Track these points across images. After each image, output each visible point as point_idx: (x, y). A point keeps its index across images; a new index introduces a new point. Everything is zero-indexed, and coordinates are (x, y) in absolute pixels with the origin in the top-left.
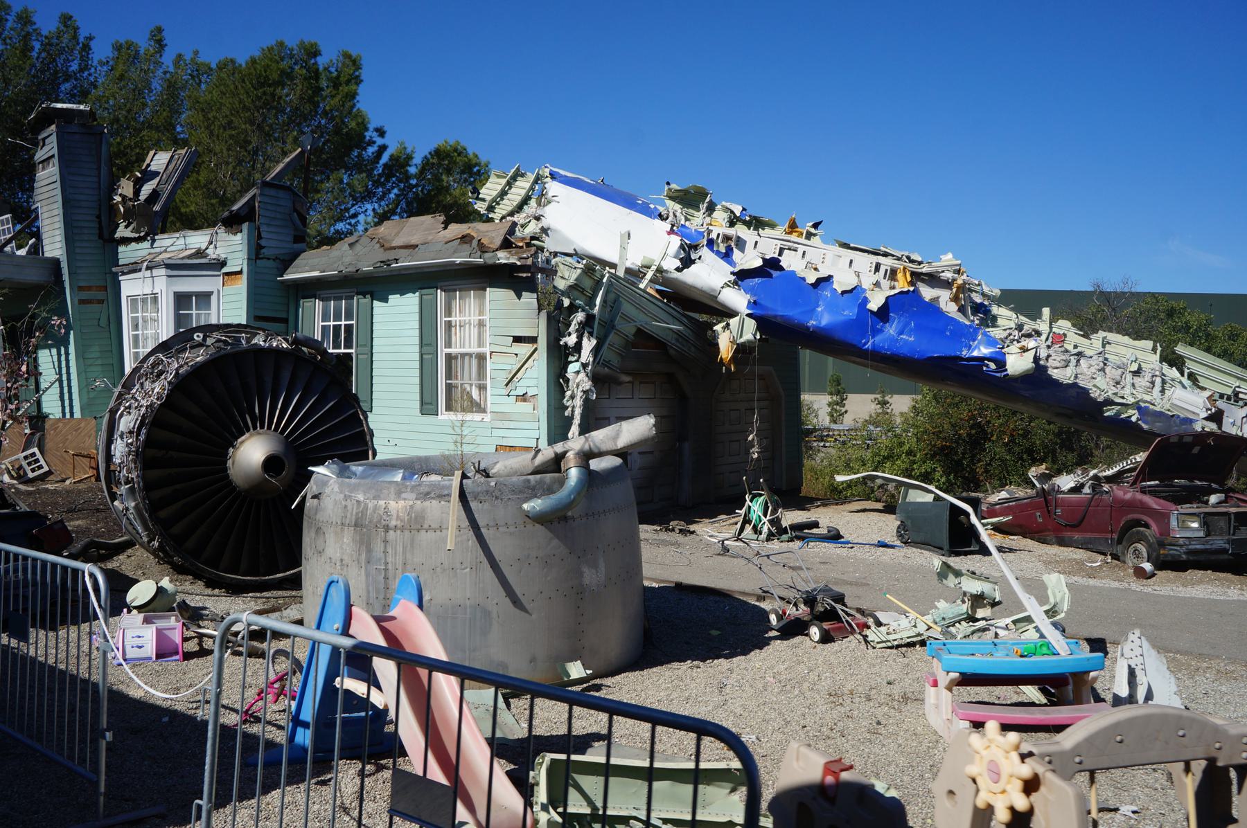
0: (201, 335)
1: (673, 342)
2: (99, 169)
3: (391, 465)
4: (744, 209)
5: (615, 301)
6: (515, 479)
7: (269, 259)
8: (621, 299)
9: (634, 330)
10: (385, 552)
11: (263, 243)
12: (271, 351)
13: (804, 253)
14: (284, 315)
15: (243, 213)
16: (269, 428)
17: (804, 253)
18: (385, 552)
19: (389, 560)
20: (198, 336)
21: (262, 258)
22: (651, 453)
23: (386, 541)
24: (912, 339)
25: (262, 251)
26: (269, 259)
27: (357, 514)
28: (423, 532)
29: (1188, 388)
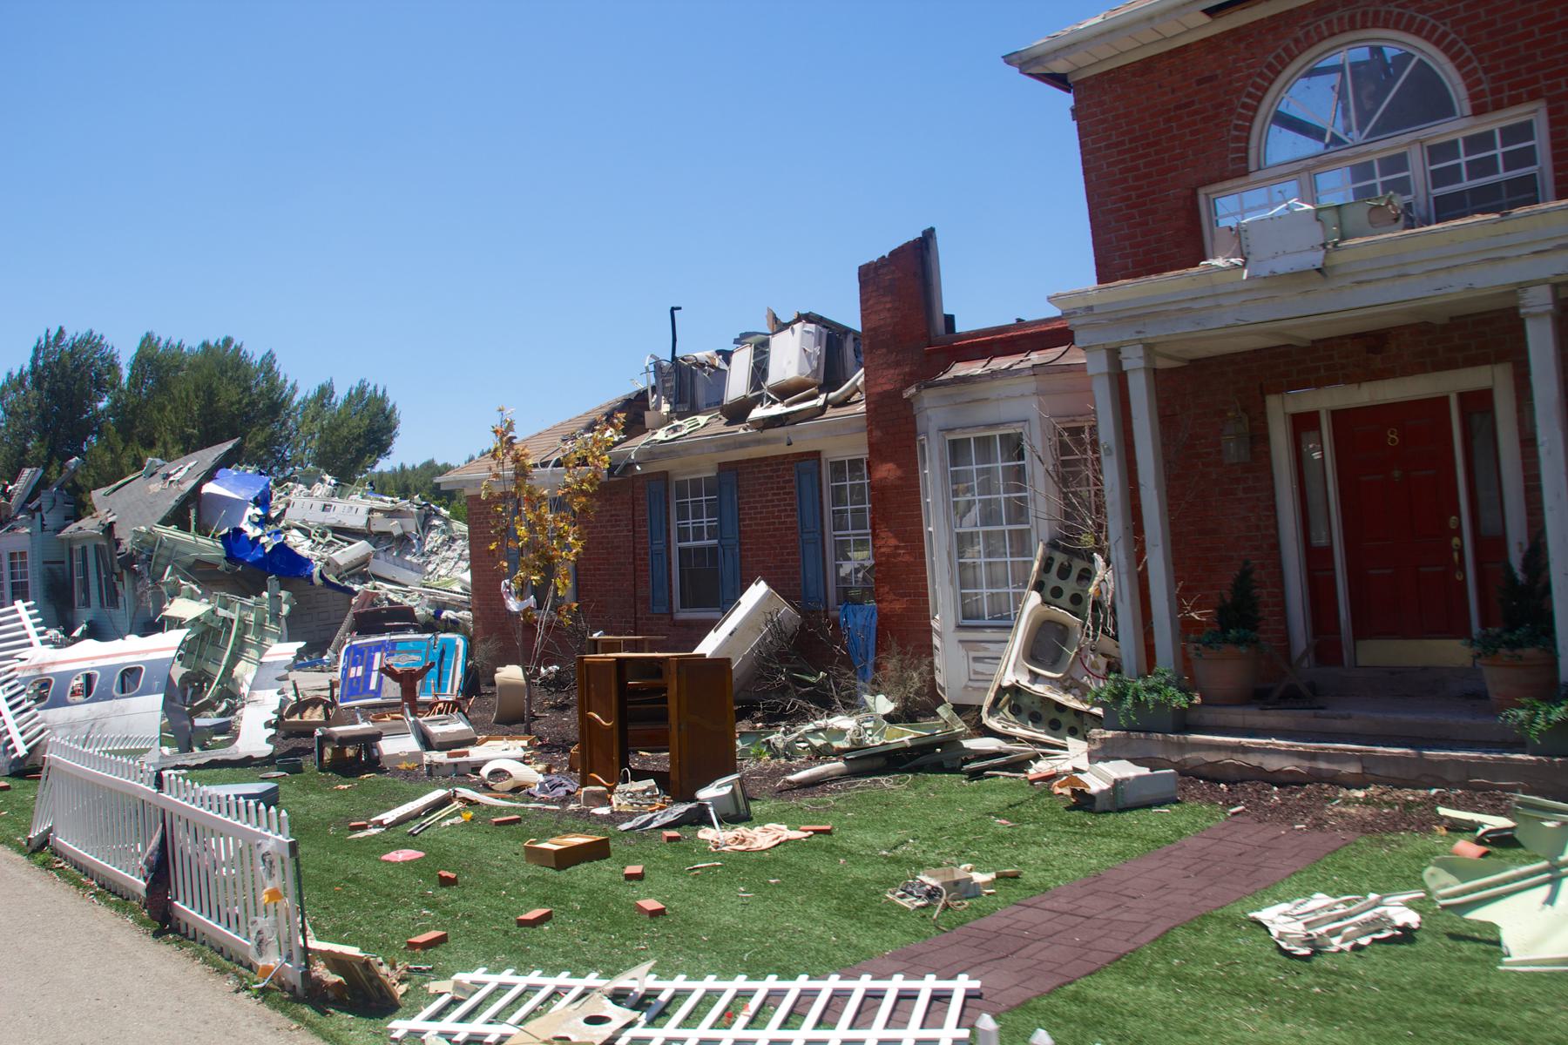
14: (61, 559)
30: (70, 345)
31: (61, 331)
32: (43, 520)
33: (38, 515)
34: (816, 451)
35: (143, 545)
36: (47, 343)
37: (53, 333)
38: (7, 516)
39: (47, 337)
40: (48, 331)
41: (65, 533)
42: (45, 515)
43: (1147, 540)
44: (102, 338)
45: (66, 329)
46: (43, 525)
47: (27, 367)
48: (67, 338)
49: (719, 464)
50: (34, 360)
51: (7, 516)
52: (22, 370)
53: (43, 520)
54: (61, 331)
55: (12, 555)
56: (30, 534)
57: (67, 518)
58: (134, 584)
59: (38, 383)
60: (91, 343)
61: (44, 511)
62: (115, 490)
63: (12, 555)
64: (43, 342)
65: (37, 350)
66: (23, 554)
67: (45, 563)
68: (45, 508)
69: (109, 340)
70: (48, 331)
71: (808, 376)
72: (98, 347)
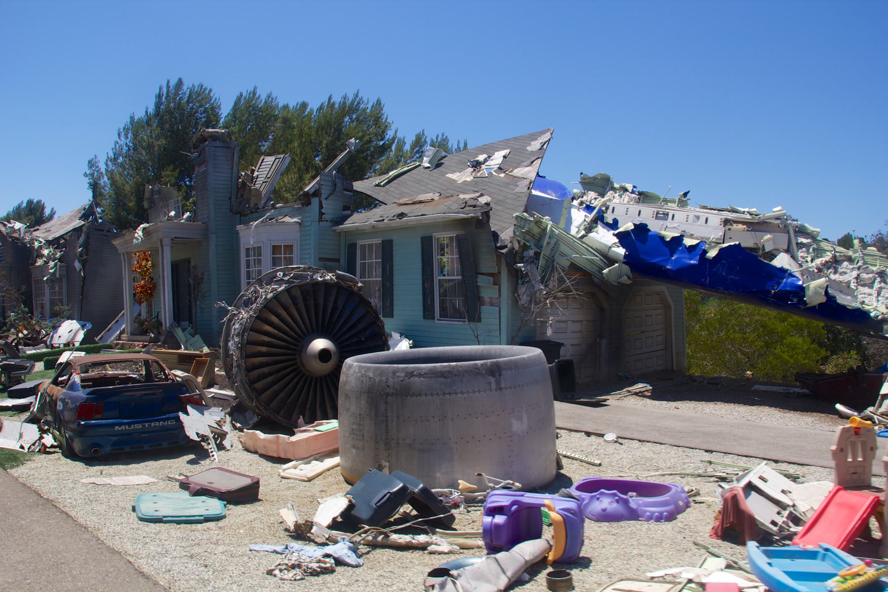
0: (282, 274)
1: (596, 273)
2: (232, 169)
3: (710, 226)
4: (634, 187)
5: (556, 243)
6: (460, 368)
7: (327, 221)
8: (560, 242)
9: (568, 263)
10: (386, 410)
11: (323, 211)
12: (325, 283)
13: (673, 216)
14: (337, 257)
15: (311, 192)
16: (299, 341)
17: (673, 216)
18: (386, 410)
19: (389, 414)
20: (280, 274)
21: (323, 221)
22: (580, 345)
23: (386, 403)
24: (737, 278)
25: (323, 216)
26: (327, 221)
27: (369, 385)
28: (409, 397)
29: (227, 512)
30: (188, 93)
31: (180, 83)
32: (321, 207)
33: (315, 201)
34: (480, 318)
35: (528, 237)
36: (168, 91)
37: (173, 83)
38: (256, 204)
39: (168, 87)
40: (168, 82)
41: (349, 224)
42: (324, 202)
43: (204, 433)
44: (211, 91)
45: (184, 80)
46: (321, 214)
47: (152, 109)
48: (185, 88)
49: (424, 318)
50: (158, 105)
51: (256, 204)
52: (147, 112)
53: (321, 207)
54: (180, 83)
55: (276, 249)
56: (300, 224)
57: (346, 208)
58: (515, 290)
59: (161, 125)
60: (201, 96)
61: (323, 196)
62: (390, 181)
63: (276, 249)
64: (165, 90)
65: (159, 96)
66: (288, 248)
67: (321, 259)
68: (325, 192)
69: (216, 94)
70: (168, 82)
71: (83, 327)
72: (208, 98)
